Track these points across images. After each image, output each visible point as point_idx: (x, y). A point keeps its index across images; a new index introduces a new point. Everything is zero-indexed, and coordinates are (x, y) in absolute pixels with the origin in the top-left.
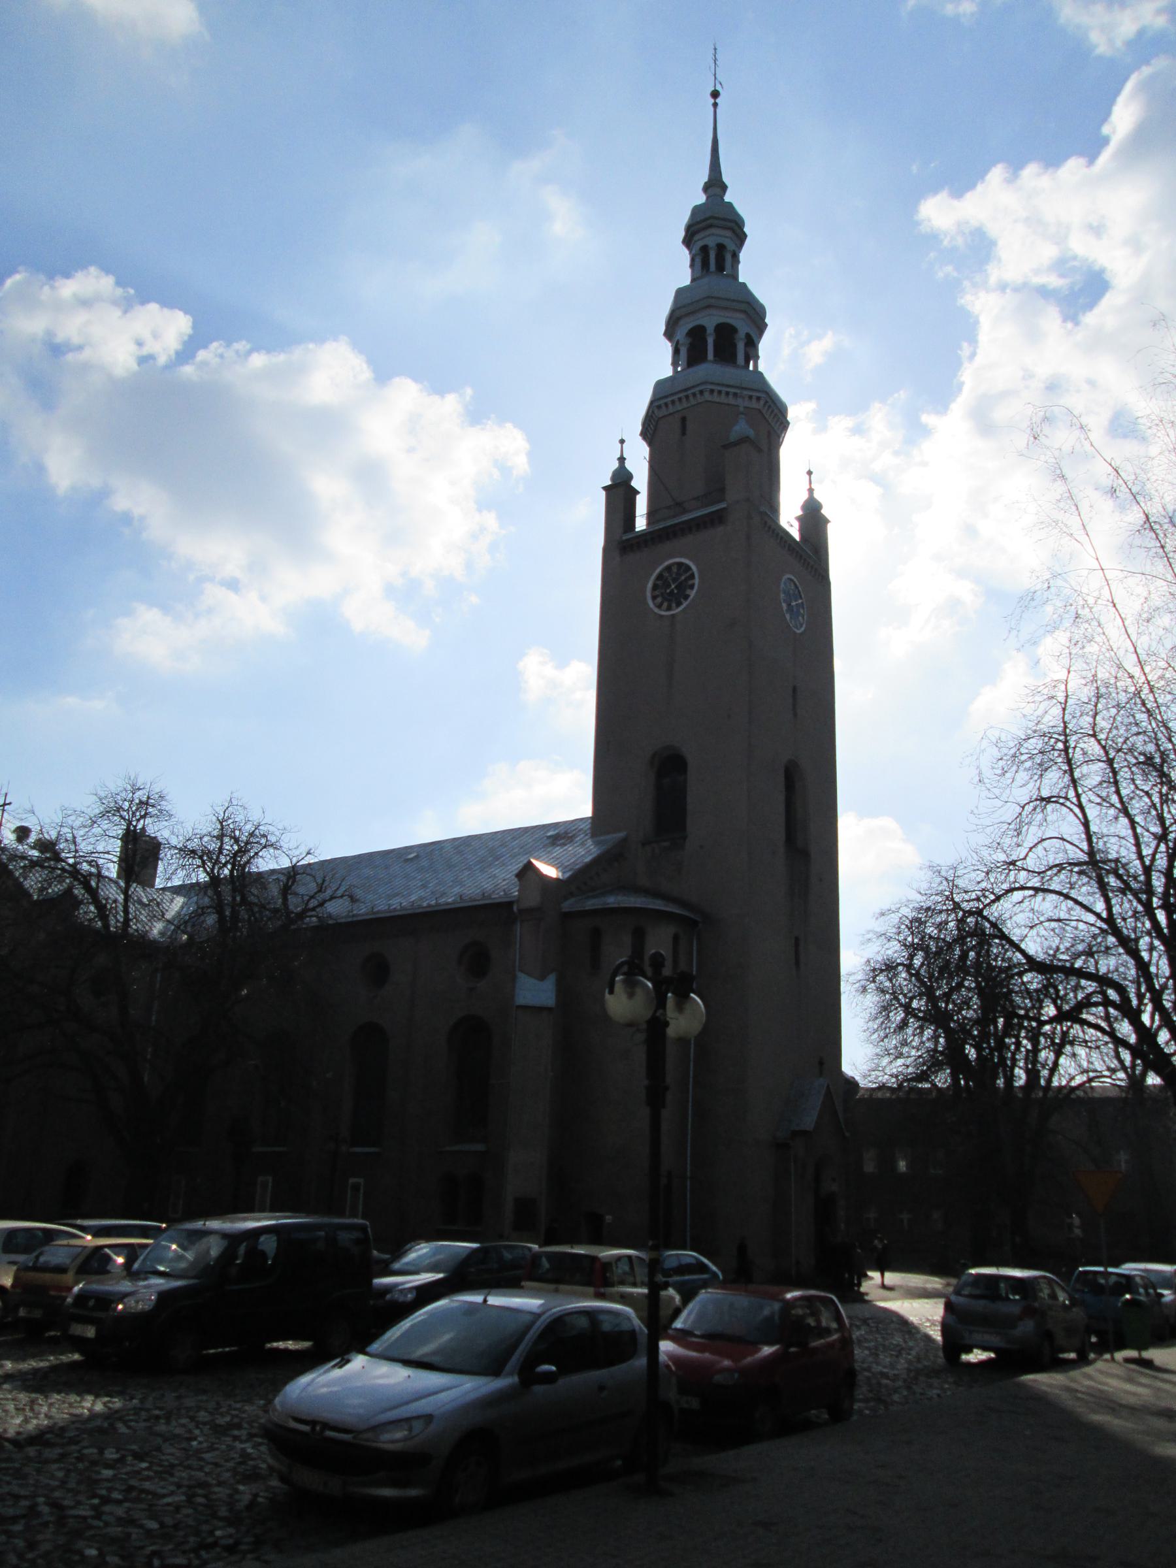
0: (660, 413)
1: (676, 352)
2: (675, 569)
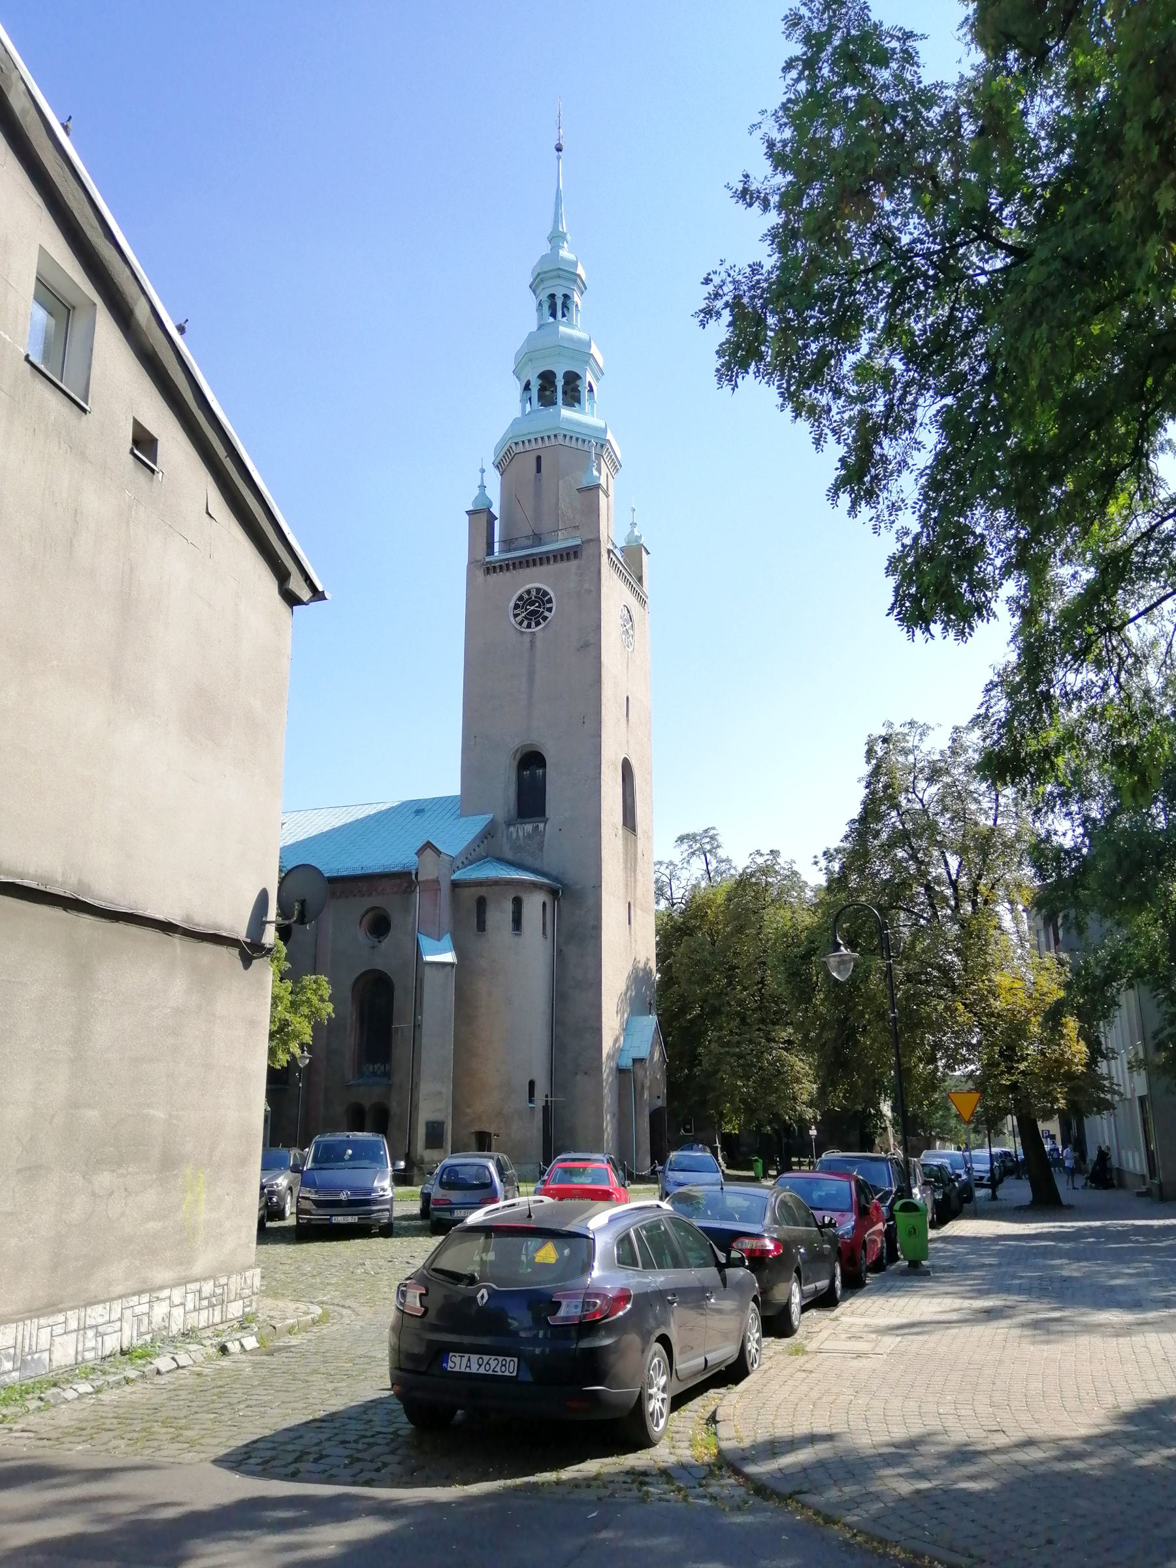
0: (516, 450)
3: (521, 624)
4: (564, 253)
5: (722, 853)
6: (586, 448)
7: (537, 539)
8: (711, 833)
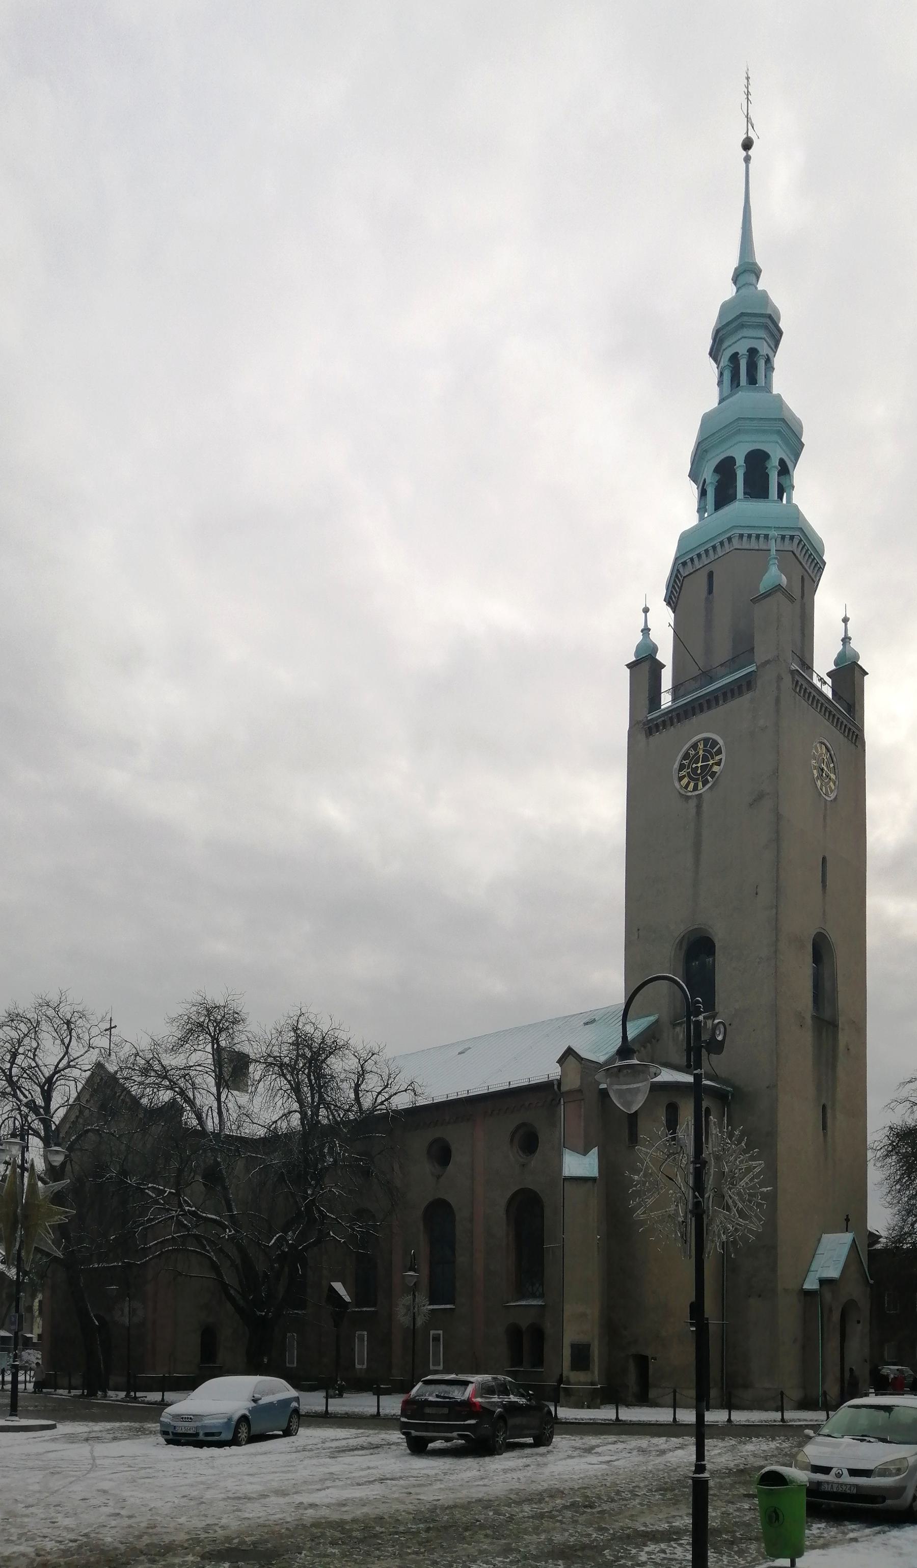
1: (703, 493)
2: (701, 746)
3: (687, 786)
6: (762, 545)
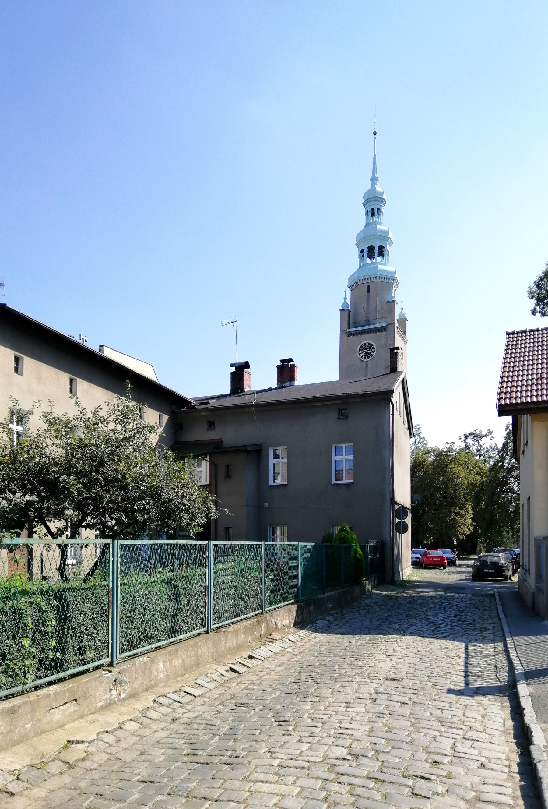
2: (367, 345)
3: (362, 357)
4: (379, 189)
5: (421, 435)
7: (368, 322)
8: (418, 427)
